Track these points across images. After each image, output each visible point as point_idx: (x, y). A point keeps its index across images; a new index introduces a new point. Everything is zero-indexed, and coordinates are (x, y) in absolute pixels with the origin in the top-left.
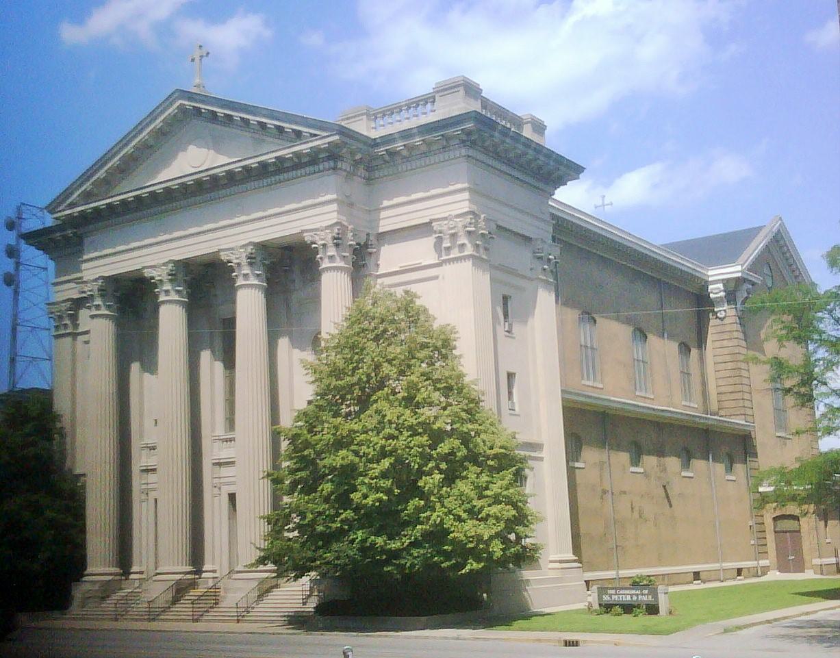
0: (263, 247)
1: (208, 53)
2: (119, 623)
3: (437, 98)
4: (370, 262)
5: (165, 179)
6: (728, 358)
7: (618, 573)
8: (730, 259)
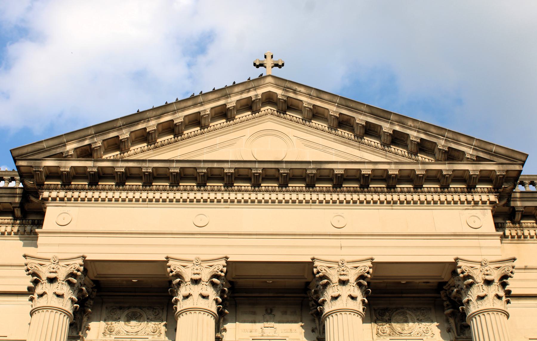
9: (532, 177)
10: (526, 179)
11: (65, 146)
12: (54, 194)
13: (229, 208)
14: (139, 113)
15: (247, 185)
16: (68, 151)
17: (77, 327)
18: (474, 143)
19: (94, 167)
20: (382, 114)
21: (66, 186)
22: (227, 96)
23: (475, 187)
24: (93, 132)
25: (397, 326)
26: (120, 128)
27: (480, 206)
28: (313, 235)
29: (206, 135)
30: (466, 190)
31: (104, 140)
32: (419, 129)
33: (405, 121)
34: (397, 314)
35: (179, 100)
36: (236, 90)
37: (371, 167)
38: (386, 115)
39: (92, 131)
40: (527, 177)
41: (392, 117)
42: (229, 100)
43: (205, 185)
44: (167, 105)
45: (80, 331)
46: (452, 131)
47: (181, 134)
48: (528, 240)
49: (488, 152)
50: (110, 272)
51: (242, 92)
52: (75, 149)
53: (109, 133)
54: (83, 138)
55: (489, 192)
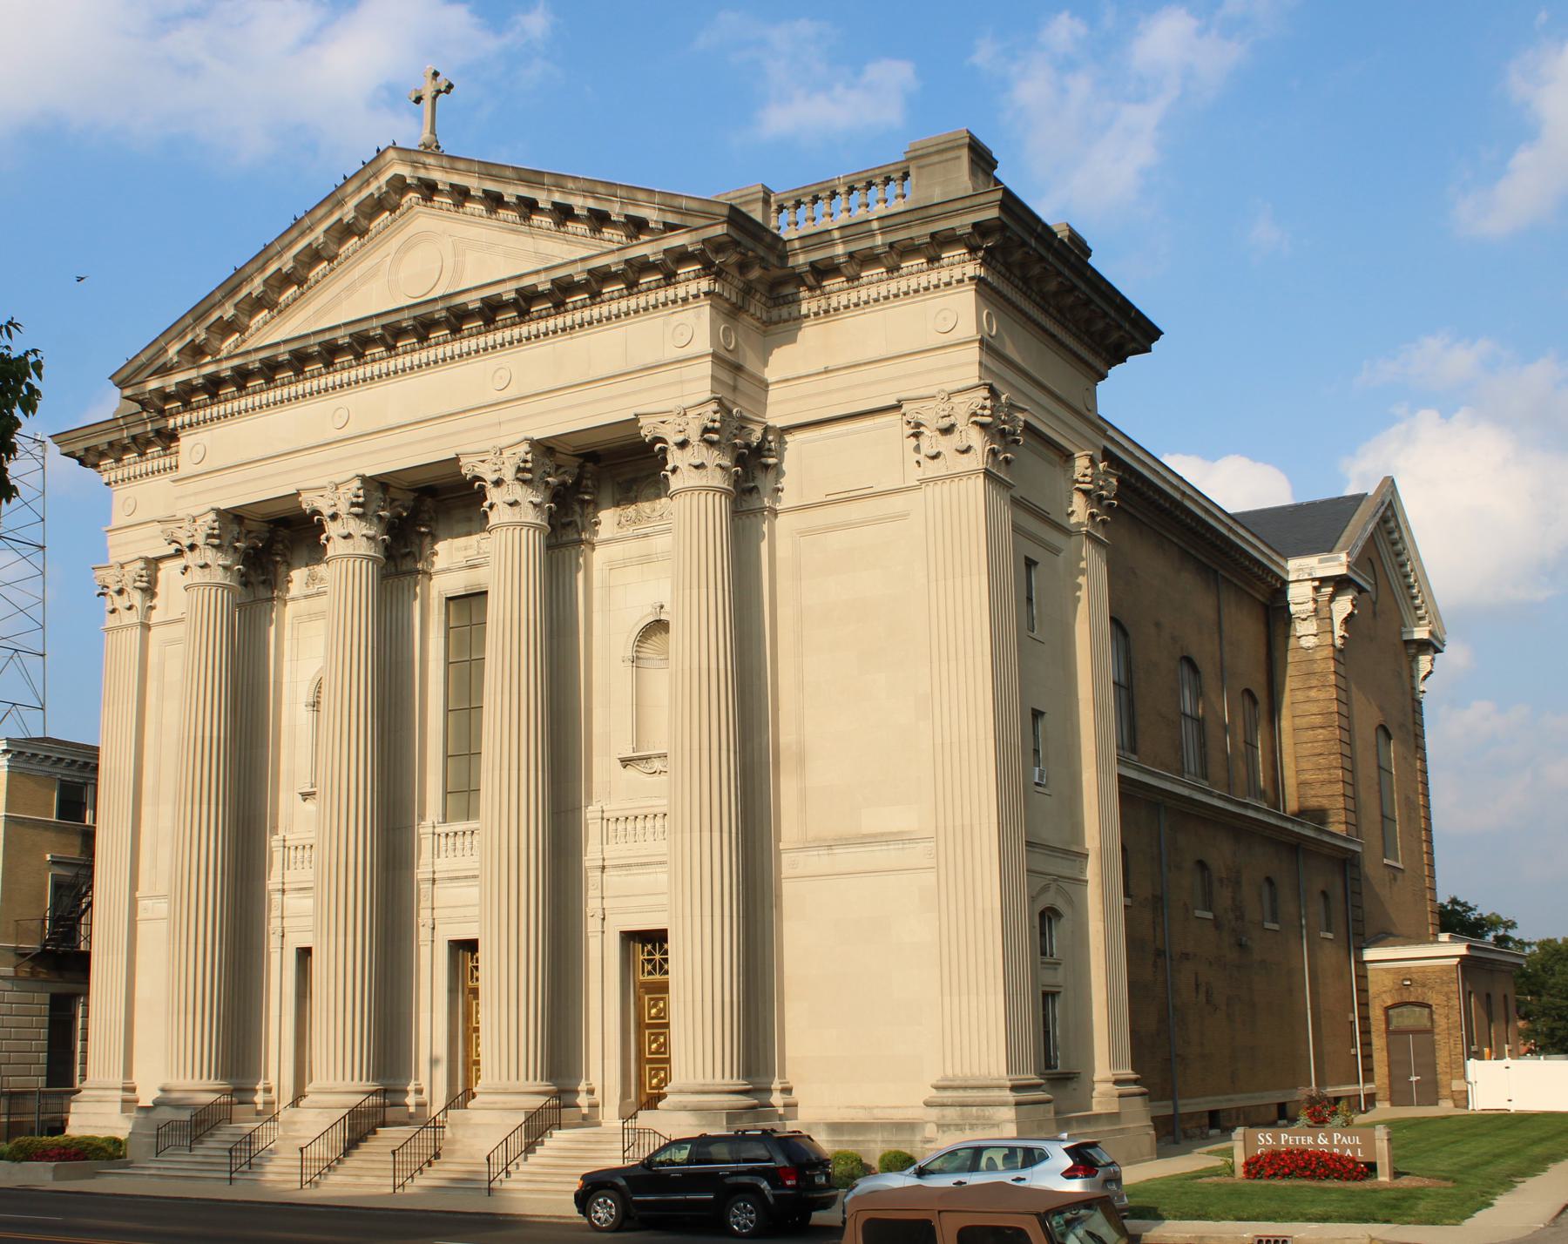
0: (545, 449)
2: (955, 1180)
3: (912, 172)
4: (765, 482)
6: (1318, 720)
7: (1175, 1108)
9: (886, 170)
11: (166, 351)
12: (179, 420)
13: (371, 388)
14: (238, 271)
15: (379, 351)
16: (171, 359)
17: (271, 584)
18: (657, 199)
19: (198, 377)
20: (533, 178)
21: (187, 406)
22: (340, 203)
23: (675, 274)
25: (645, 506)
26: (220, 304)
27: (692, 303)
32: (583, 191)
33: (563, 182)
35: (308, 210)
36: (350, 188)
37: (515, 285)
38: (538, 179)
39: (189, 320)
41: (546, 180)
42: (346, 209)
43: (332, 364)
45: (275, 589)
47: (306, 280)
48: (842, 313)
49: (678, 211)
50: (277, 508)
51: (359, 189)
52: (179, 352)
53: (210, 315)
54: (182, 334)
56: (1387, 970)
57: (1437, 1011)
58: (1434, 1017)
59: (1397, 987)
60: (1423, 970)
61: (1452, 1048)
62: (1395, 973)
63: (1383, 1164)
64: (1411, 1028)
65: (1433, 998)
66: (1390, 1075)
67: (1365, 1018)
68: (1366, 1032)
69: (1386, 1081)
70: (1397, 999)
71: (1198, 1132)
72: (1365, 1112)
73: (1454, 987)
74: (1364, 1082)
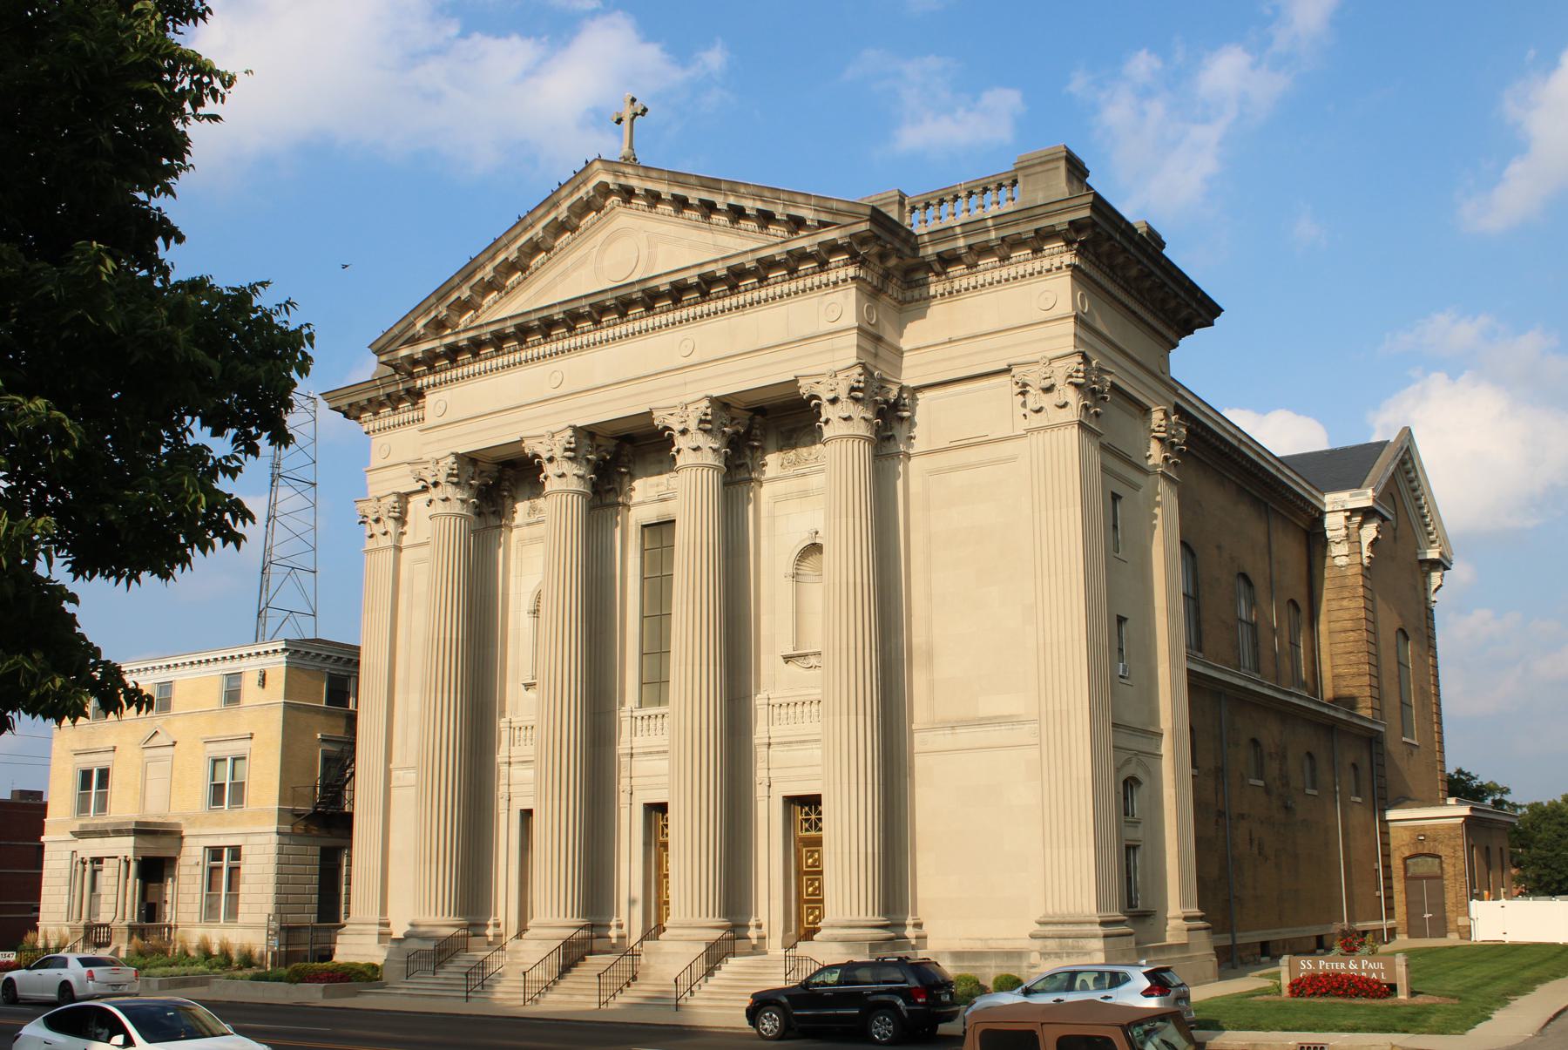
0: (722, 405)
1: (645, 110)
4: (900, 431)
5: (566, 299)
8: (1355, 483)
9: (998, 178)
10: (990, 183)
16: (419, 331)
19: (441, 346)
20: (712, 184)
21: (432, 369)
22: (556, 205)
24: (435, 301)
25: (803, 451)
26: (459, 287)
28: (656, 374)
29: (554, 260)
30: (817, 269)
31: (448, 307)
33: (736, 188)
34: (804, 435)
36: (564, 193)
37: (697, 271)
40: (992, 179)
41: (723, 186)
42: (560, 210)
43: (550, 335)
44: (496, 241)
46: (788, 191)
47: (528, 267)
48: (963, 294)
51: (571, 194)
52: (425, 326)
54: (428, 311)
55: (846, 265)
56: (1405, 828)
57: (1446, 861)
58: (1444, 865)
59: (1413, 841)
60: (1434, 827)
61: (1458, 890)
62: (1412, 830)
63: (1402, 985)
64: (1425, 875)
65: (1443, 851)
66: (1407, 913)
67: (1387, 867)
68: (1388, 878)
69: (1405, 917)
70: (1414, 851)
71: (1252, 959)
72: (1387, 943)
73: (1460, 841)
74: (1387, 918)
